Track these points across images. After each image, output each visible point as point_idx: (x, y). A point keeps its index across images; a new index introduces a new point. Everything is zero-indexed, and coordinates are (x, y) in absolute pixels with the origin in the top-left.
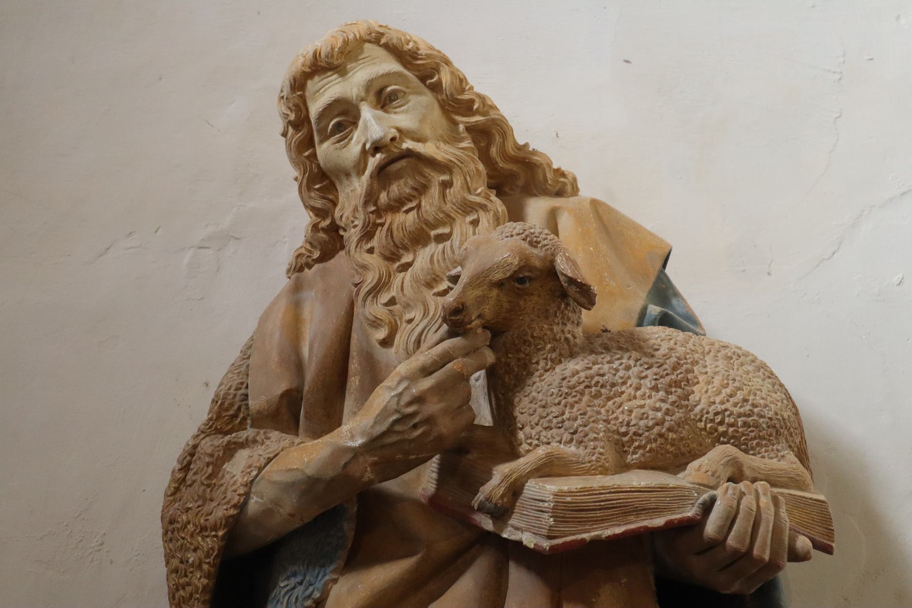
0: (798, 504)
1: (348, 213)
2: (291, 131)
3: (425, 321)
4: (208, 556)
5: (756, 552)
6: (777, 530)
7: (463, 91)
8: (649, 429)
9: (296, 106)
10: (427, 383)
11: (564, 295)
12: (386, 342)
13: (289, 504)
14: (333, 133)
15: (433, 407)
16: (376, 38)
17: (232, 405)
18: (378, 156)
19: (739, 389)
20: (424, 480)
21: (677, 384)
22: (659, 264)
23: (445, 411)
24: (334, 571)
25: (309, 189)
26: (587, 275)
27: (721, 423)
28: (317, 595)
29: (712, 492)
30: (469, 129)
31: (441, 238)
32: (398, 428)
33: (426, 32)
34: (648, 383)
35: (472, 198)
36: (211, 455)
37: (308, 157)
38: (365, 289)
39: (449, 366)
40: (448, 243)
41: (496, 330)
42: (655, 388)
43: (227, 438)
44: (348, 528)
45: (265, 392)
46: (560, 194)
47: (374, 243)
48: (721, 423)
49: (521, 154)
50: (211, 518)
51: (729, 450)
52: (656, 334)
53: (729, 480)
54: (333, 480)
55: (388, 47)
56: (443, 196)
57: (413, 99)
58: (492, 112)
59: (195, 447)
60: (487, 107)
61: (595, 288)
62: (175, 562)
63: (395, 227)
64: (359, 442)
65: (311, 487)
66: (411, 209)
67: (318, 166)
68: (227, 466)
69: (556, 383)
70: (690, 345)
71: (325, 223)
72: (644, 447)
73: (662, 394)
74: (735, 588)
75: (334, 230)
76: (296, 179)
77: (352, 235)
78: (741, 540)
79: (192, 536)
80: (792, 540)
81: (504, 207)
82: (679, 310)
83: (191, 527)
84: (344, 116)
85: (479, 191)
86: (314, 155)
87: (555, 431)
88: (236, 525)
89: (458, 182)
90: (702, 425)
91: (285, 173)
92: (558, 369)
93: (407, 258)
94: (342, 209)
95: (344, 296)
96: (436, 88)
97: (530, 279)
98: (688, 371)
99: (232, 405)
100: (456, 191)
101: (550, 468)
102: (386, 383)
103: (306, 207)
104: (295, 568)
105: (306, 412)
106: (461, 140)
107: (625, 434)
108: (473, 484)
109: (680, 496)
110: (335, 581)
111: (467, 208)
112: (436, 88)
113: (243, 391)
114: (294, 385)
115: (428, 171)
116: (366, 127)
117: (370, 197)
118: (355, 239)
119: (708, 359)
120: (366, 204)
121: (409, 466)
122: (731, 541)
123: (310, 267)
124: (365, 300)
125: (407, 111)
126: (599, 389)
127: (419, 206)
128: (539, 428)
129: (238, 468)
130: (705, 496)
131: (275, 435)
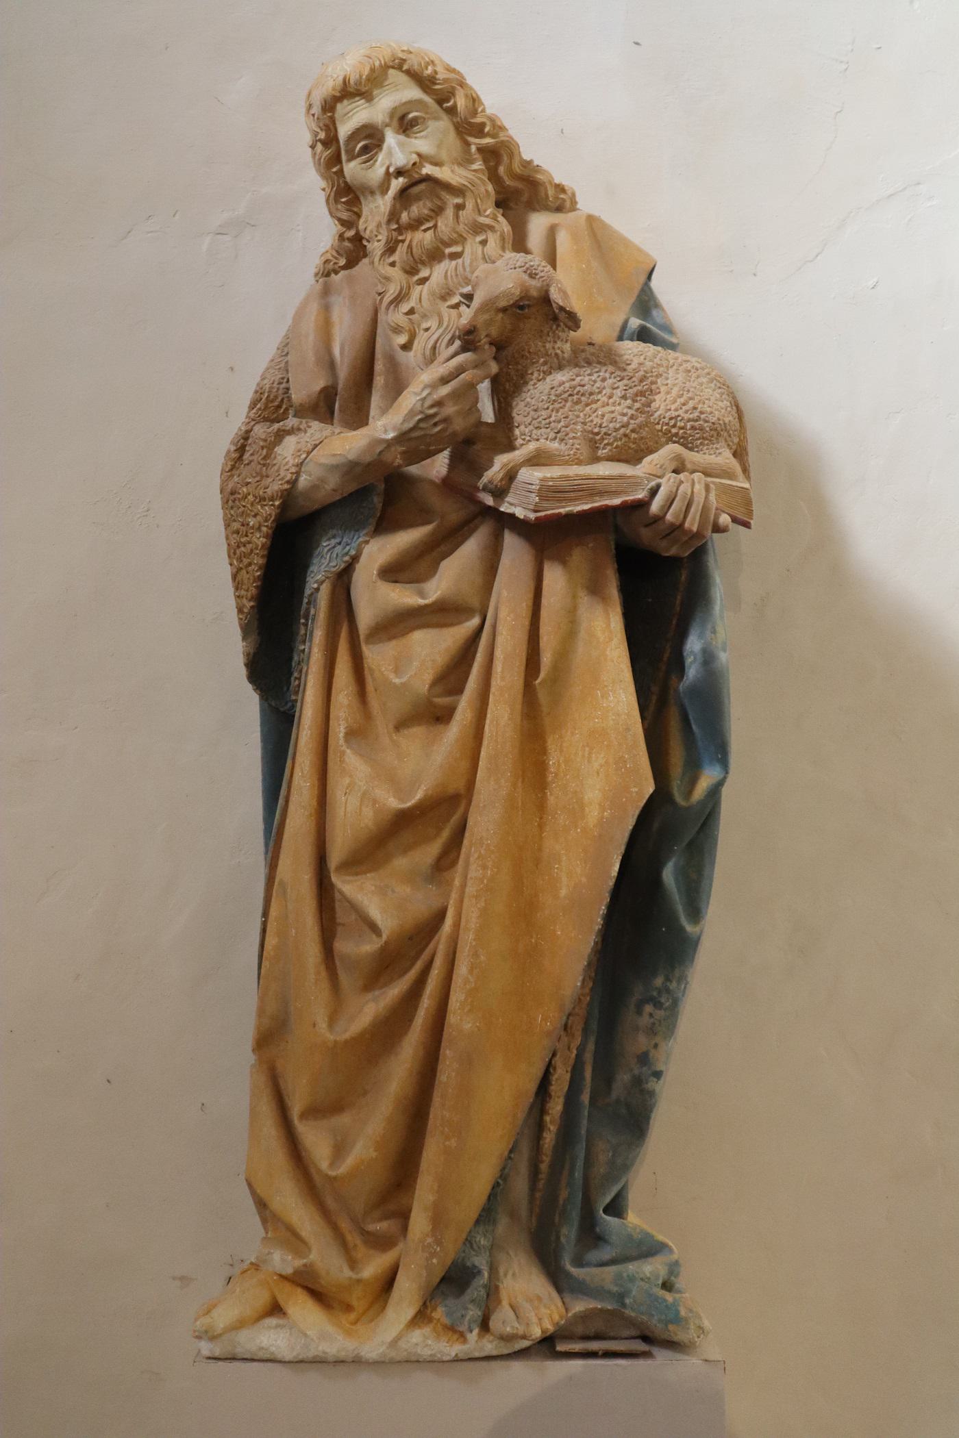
0: (724, 490)
1: (371, 226)
2: (319, 147)
3: (441, 331)
4: (266, 521)
5: (687, 525)
6: (705, 509)
7: (475, 113)
8: (616, 430)
9: (326, 126)
10: (445, 390)
11: (555, 319)
12: (406, 347)
13: (333, 482)
14: (359, 155)
15: (450, 410)
16: (399, 65)
17: (276, 397)
18: (401, 179)
19: (691, 399)
20: (438, 466)
21: (642, 394)
22: (643, 279)
23: (458, 413)
24: (366, 534)
25: (336, 201)
26: (576, 305)
27: (674, 426)
28: (353, 552)
29: (659, 480)
30: (480, 150)
31: (455, 256)
32: (422, 425)
33: (445, 50)
34: (618, 393)
35: (482, 220)
36: (265, 440)
37: (335, 173)
38: (387, 299)
39: (463, 376)
40: (460, 261)
41: (499, 346)
42: (624, 397)
43: (276, 426)
44: (377, 501)
45: (306, 387)
46: (559, 209)
47: (395, 257)
48: (674, 426)
49: (526, 173)
50: (269, 491)
51: (672, 448)
52: (631, 349)
53: (674, 471)
54: (369, 464)
55: (409, 73)
56: (457, 217)
57: (432, 125)
58: (501, 134)
59: (248, 432)
60: (498, 128)
61: (580, 315)
62: (236, 526)
63: (414, 244)
64: (391, 435)
65: (351, 468)
66: (429, 229)
67: (346, 183)
68: (278, 450)
69: (546, 392)
70: (657, 360)
71: (351, 233)
72: (611, 444)
73: (629, 402)
74: (673, 551)
75: (358, 239)
76: (324, 190)
77: (376, 247)
78: (676, 516)
79: (252, 504)
80: (717, 517)
81: (509, 228)
82: (659, 320)
83: (251, 498)
84: (370, 140)
85: (488, 212)
86: (341, 171)
87: (543, 430)
88: (288, 497)
89: (470, 205)
90: (658, 427)
91: (312, 186)
92: (549, 379)
93: (424, 273)
94: (366, 222)
95: (369, 303)
96: (452, 111)
97: (529, 306)
98: (652, 383)
99: (276, 397)
100: (467, 214)
101: (536, 460)
102: (411, 389)
103: (331, 213)
104: (334, 531)
105: (340, 406)
106: (471, 162)
107: (597, 434)
108: (478, 469)
109: (635, 483)
110: (367, 542)
111: (478, 228)
112: (452, 111)
113: (284, 385)
114: (330, 383)
115: (444, 194)
116: (390, 154)
117: (393, 216)
118: (378, 253)
119: (671, 372)
120: (389, 221)
121: (430, 454)
122: (669, 517)
123: (336, 273)
124: (388, 308)
125: (426, 137)
126: (577, 396)
127: (435, 226)
128: (531, 427)
129: (288, 450)
130: (653, 484)
131: (316, 425)
